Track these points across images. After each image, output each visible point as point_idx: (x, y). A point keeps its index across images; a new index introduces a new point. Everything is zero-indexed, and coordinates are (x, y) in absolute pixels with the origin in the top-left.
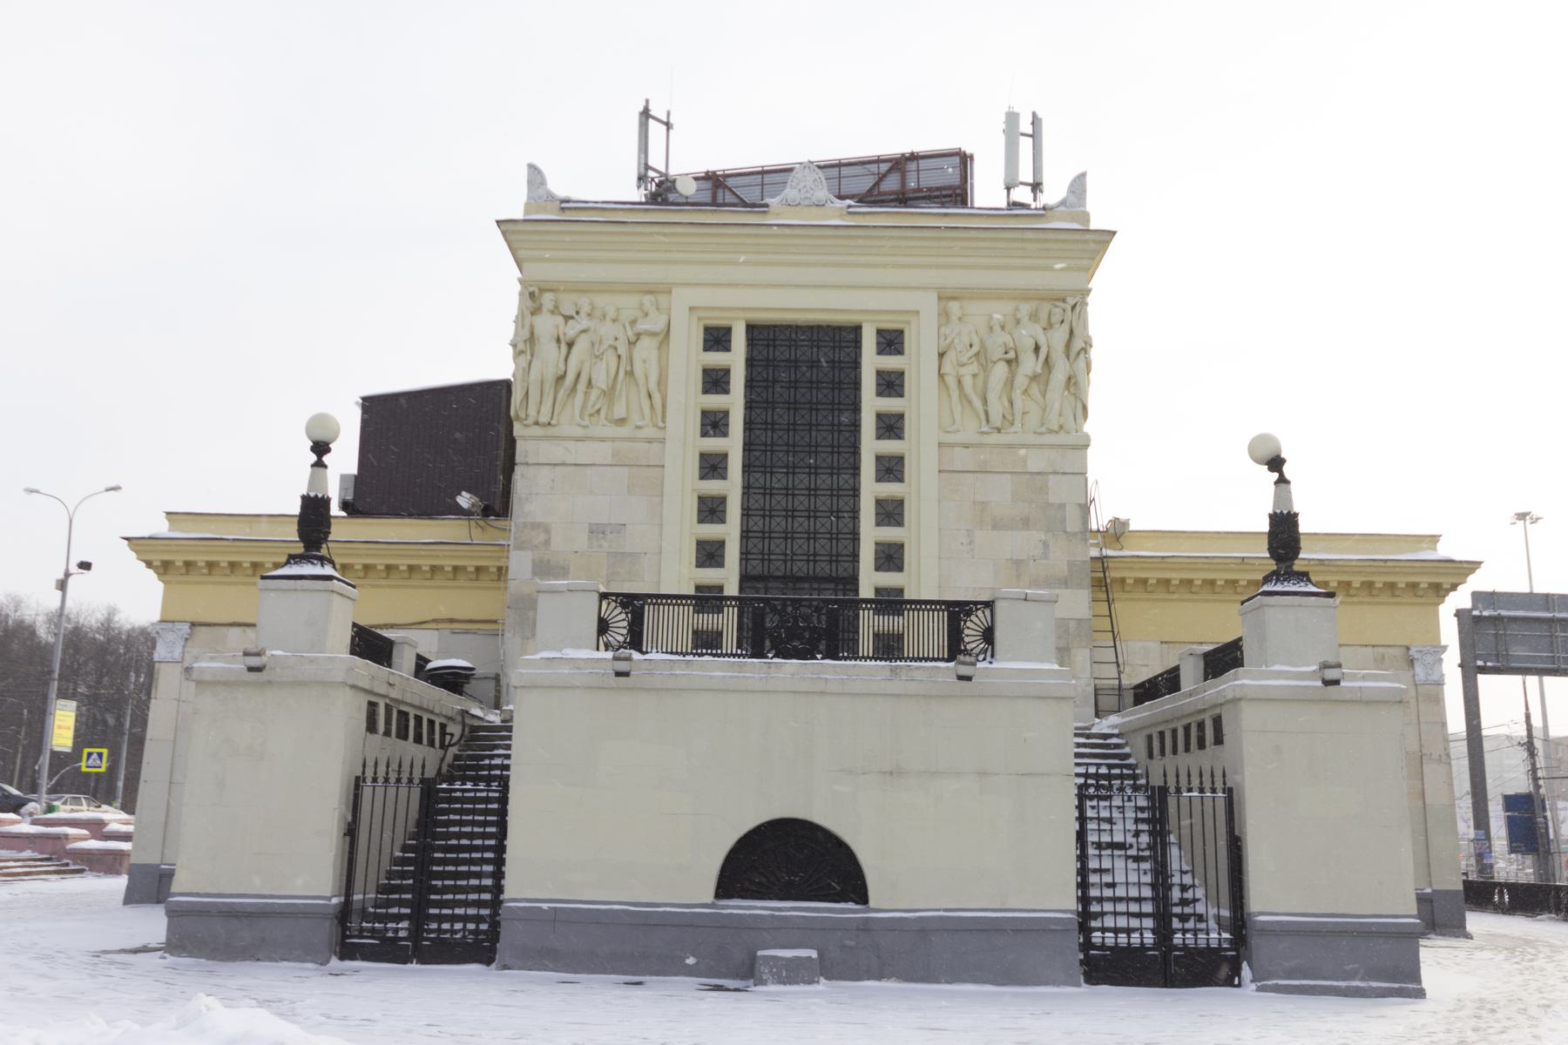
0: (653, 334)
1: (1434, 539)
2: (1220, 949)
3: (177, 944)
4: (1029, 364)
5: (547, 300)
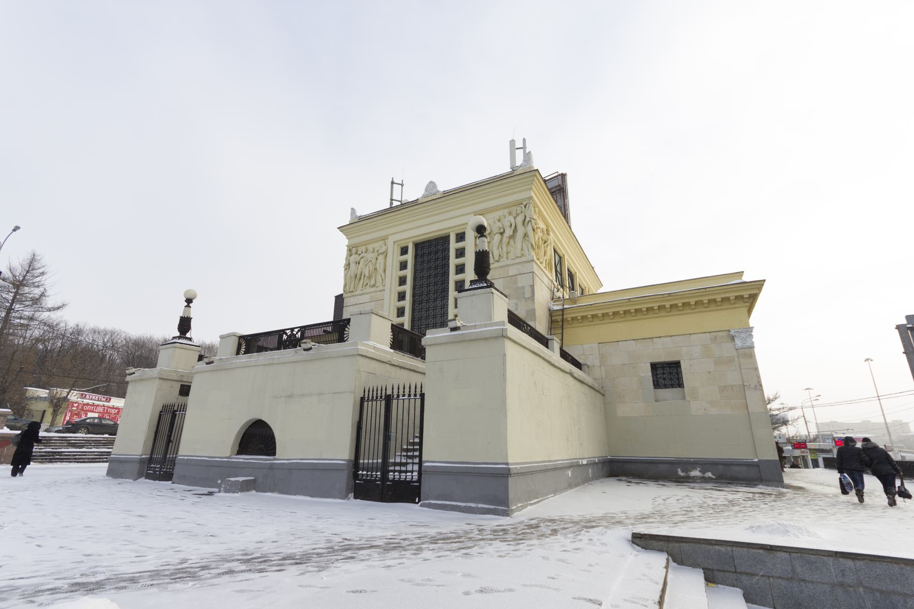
1: (741, 274)
2: (411, 481)
3: (111, 473)
4: (509, 232)
5: (354, 250)
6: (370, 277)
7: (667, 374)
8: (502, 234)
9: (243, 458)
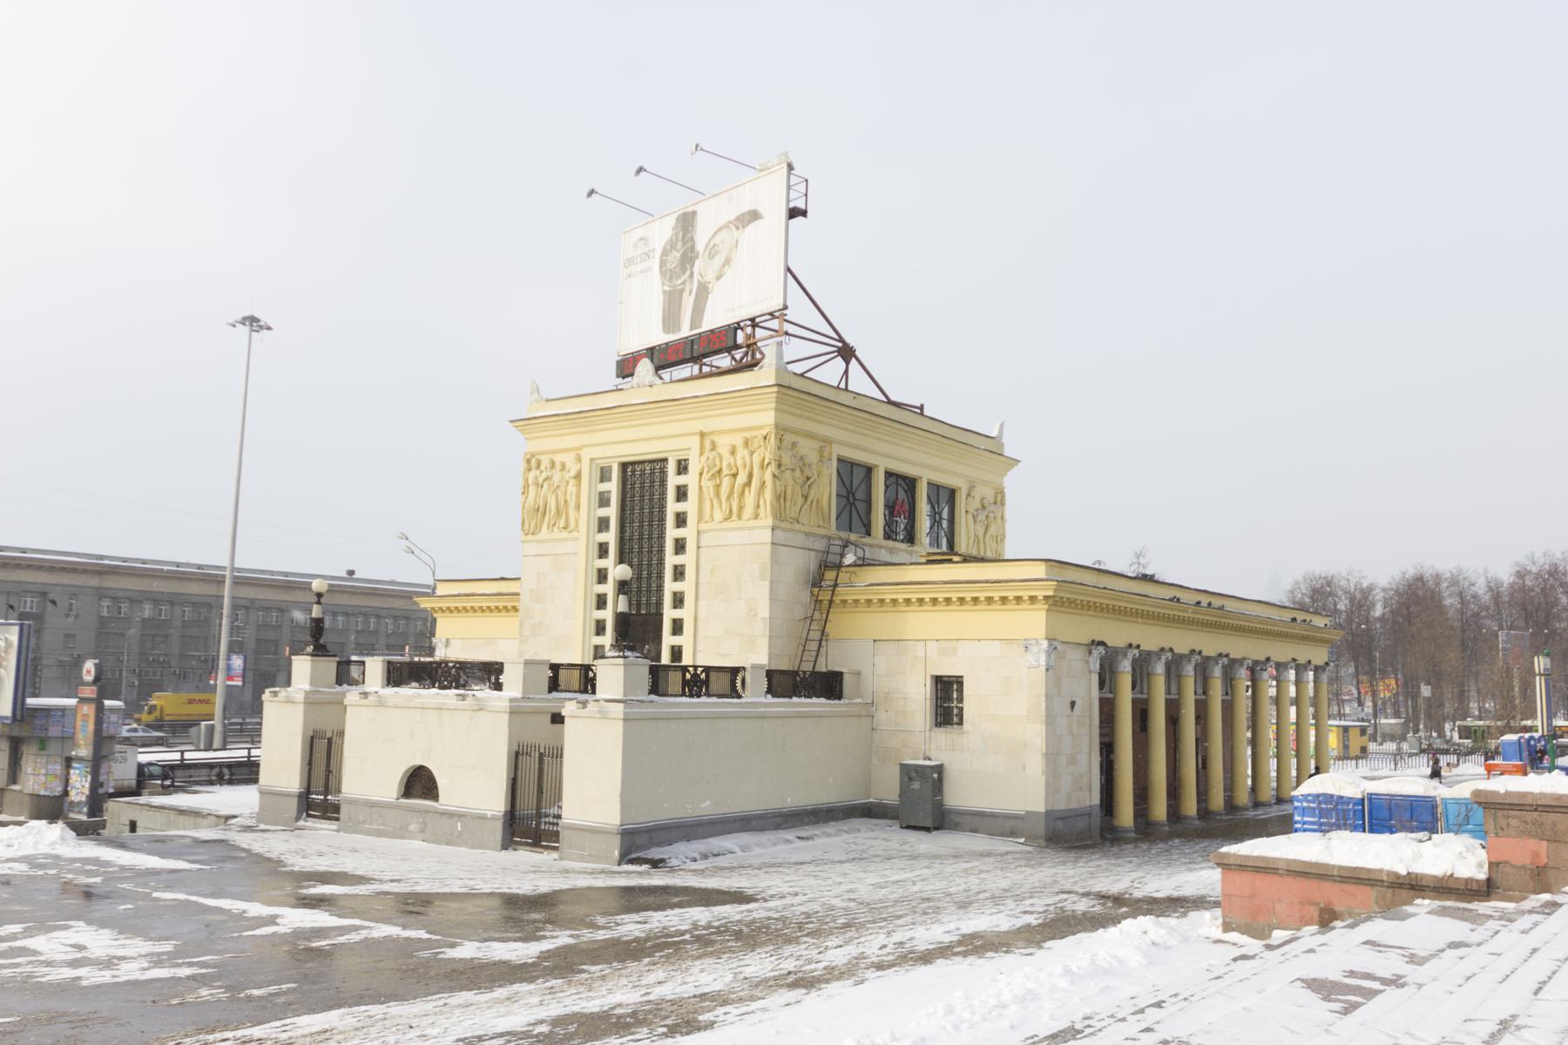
7: (133, 826)
8: (735, 476)
9: (403, 801)
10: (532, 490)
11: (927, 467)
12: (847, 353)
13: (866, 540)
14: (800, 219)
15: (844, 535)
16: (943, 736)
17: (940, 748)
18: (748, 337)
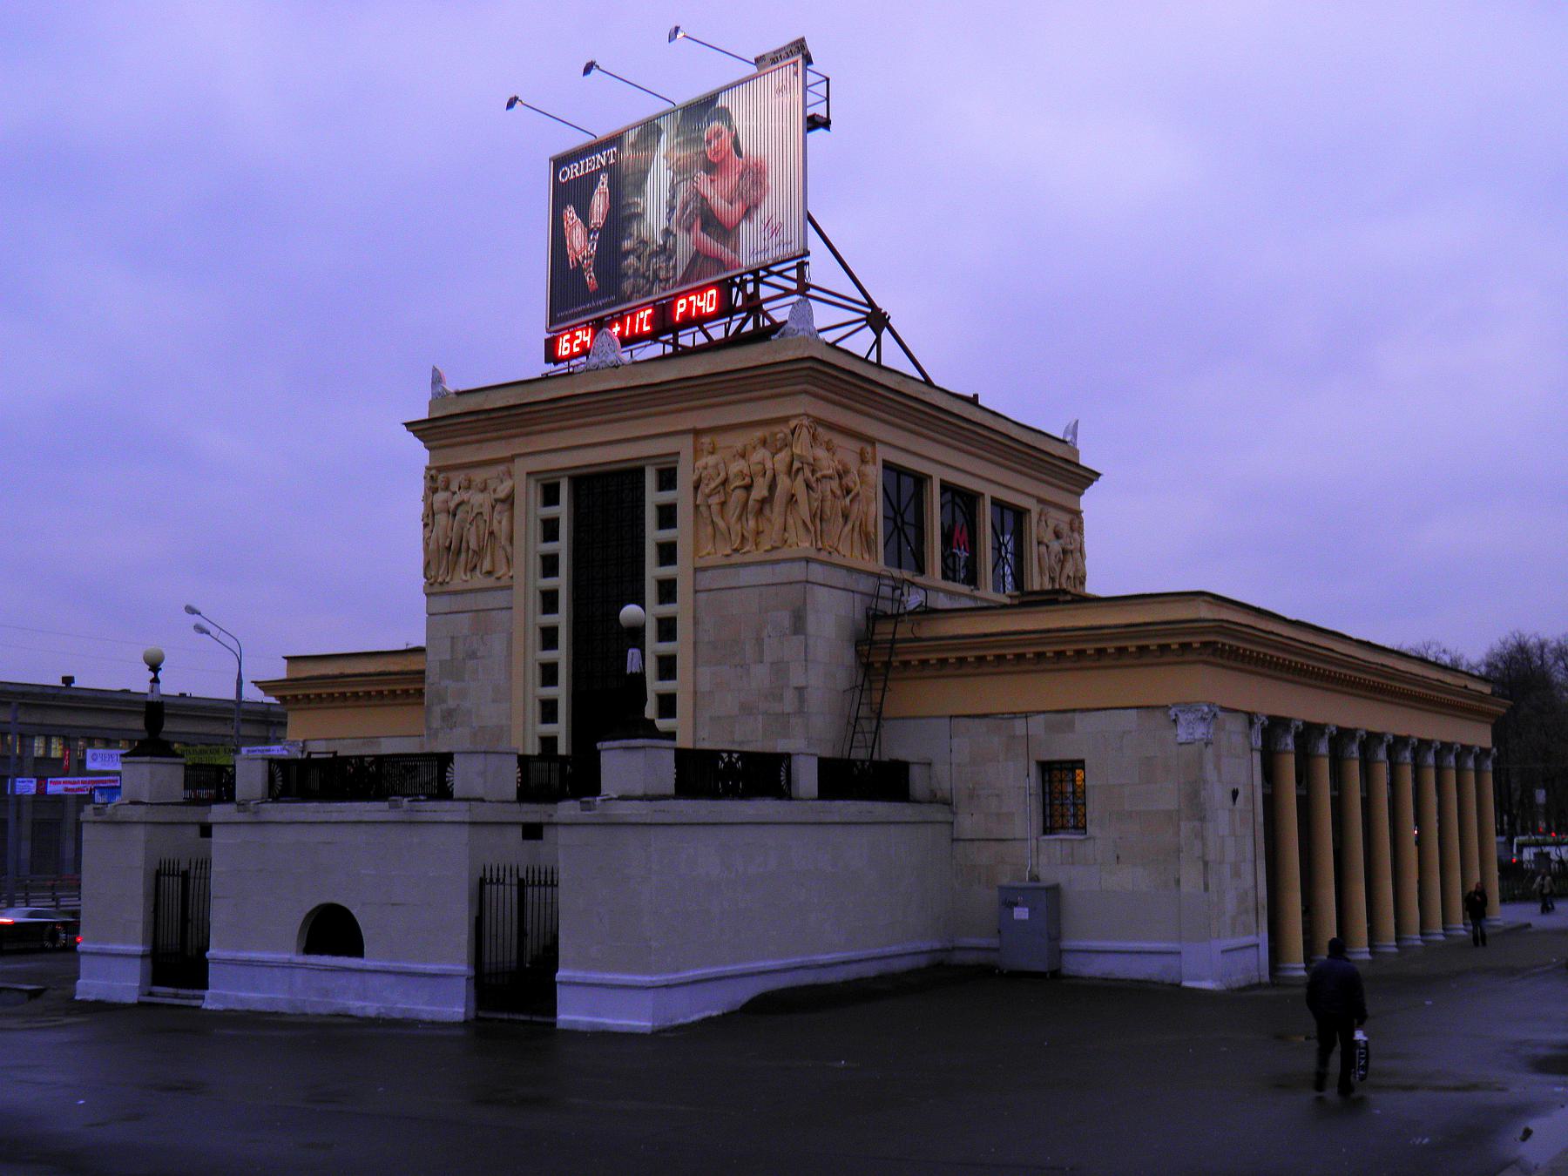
0: (503, 501)
4: (759, 491)
6: (479, 553)
8: (748, 488)
10: (442, 519)
11: (991, 481)
12: (877, 320)
13: (918, 579)
14: (821, 131)
15: (896, 573)
16: (1056, 845)
17: (1052, 860)
18: (747, 298)
